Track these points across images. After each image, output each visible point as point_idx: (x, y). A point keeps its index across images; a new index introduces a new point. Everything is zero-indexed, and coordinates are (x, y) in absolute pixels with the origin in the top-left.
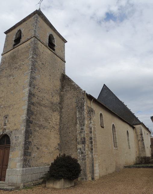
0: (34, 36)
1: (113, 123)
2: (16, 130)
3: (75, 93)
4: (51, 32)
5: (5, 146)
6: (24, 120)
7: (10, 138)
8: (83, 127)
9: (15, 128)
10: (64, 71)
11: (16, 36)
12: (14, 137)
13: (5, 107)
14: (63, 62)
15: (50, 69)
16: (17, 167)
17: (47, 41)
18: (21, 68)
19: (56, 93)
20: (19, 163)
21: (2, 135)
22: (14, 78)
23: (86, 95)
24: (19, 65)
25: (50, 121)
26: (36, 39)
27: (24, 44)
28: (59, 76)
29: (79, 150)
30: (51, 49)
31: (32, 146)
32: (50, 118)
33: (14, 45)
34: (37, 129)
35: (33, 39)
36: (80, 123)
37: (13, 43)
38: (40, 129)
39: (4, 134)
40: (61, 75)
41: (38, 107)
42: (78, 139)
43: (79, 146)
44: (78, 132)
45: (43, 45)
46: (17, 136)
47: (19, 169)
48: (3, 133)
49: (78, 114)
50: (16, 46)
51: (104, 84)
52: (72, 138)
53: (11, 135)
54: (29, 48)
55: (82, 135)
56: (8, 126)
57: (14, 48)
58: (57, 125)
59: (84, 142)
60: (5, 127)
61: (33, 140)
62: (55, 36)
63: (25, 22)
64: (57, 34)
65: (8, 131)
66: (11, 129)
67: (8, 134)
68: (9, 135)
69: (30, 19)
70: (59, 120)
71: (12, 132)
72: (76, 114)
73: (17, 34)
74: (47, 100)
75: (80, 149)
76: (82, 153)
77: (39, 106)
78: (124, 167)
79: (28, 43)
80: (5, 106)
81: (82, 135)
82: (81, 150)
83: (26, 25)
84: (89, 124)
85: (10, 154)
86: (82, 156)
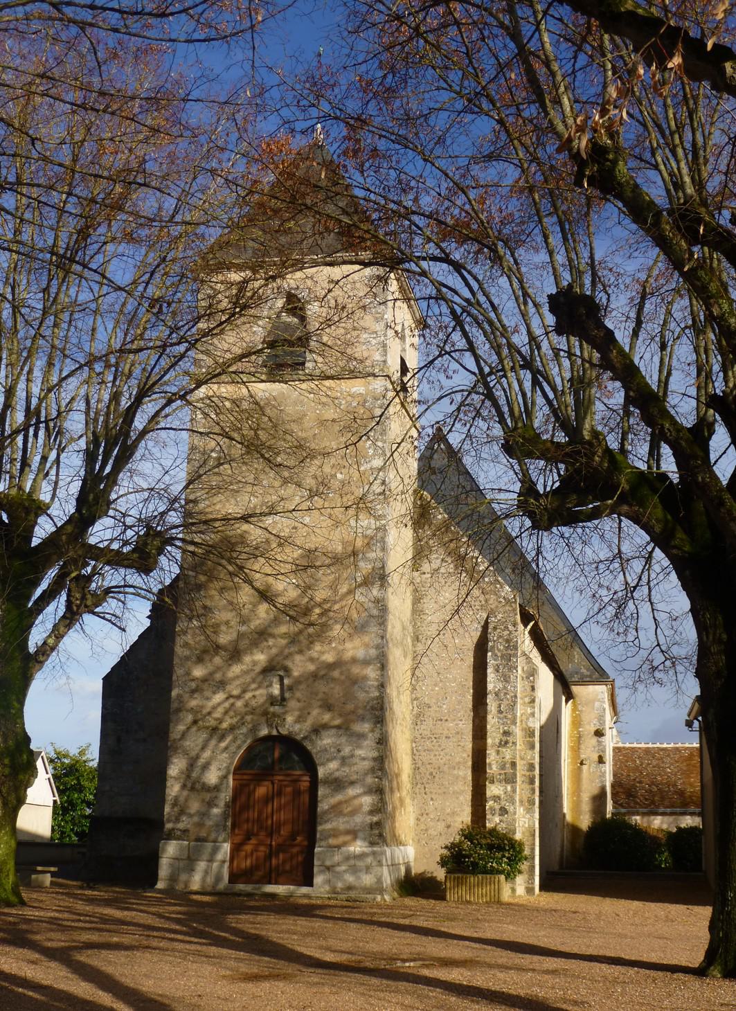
36: (500, 712)
84: (528, 719)
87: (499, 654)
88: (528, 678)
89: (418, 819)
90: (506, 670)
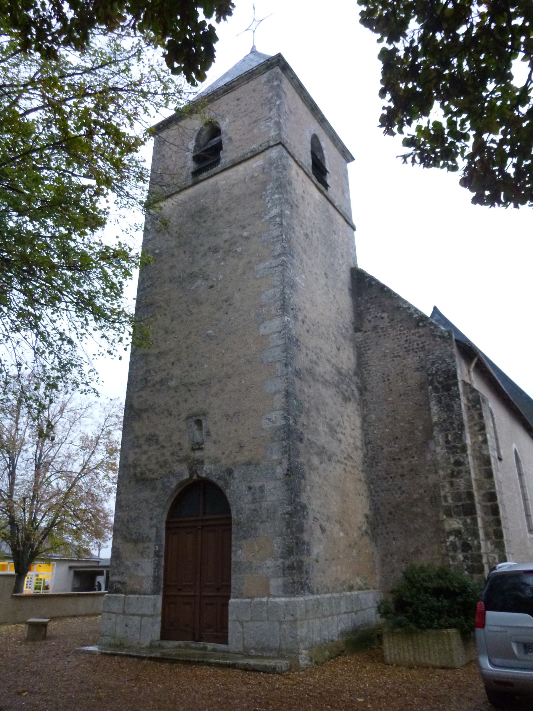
0: (280, 143)
1: (514, 446)
2: (249, 464)
3: (414, 338)
4: (315, 128)
5: (202, 520)
6: (280, 429)
7: (227, 493)
9: (246, 455)
10: (355, 259)
11: (197, 140)
13: (185, 385)
14: (350, 229)
15: (323, 254)
16: (272, 591)
17: (307, 160)
18: (239, 250)
19: (344, 337)
20: (280, 581)
21: (187, 480)
22: (210, 283)
23: (454, 344)
24: (226, 241)
25: (340, 436)
26: (285, 153)
27: (241, 168)
28: (345, 277)
30: (320, 185)
31: (311, 521)
32: (338, 425)
33: (196, 173)
34: (316, 461)
35: (274, 153)
36: (447, 442)
37: (191, 165)
38: (321, 463)
39: (195, 477)
40: (349, 274)
41: (310, 387)
42: (445, 497)
43: (455, 523)
44: (441, 473)
45: (301, 172)
47: (283, 599)
48: (191, 476)
50: (205, 175)
51: (435, 308)
52: (415, 496)
53: (227, 484)
54: (264, 184)
57: (195, 184)
58: (356, 449)
60: (198, 454)
61: (309, 498)
62: (325, 143)
63: (232, 95)
64: (327, 134)
65: (213, 467)
66: (223, 462)
67: (214, 479)
68: (221, 483)
69: (253, 84)
70: (359, 431)
71: (230, 472)
72: (429, 409)
73: (200, 133)
74: (329, 361)
75: (457, 533)
76: (466, 547)
77: (312, 383)
79: (254, 165)
80: (186, 380)
82: (460, 539)
83: (238, 105)
84: (480, 447)
85: (233, 549)
86: (466, 558)
87: (439, 386)
88: (474, 406)
89: (383, 561)
90: (448, 400)
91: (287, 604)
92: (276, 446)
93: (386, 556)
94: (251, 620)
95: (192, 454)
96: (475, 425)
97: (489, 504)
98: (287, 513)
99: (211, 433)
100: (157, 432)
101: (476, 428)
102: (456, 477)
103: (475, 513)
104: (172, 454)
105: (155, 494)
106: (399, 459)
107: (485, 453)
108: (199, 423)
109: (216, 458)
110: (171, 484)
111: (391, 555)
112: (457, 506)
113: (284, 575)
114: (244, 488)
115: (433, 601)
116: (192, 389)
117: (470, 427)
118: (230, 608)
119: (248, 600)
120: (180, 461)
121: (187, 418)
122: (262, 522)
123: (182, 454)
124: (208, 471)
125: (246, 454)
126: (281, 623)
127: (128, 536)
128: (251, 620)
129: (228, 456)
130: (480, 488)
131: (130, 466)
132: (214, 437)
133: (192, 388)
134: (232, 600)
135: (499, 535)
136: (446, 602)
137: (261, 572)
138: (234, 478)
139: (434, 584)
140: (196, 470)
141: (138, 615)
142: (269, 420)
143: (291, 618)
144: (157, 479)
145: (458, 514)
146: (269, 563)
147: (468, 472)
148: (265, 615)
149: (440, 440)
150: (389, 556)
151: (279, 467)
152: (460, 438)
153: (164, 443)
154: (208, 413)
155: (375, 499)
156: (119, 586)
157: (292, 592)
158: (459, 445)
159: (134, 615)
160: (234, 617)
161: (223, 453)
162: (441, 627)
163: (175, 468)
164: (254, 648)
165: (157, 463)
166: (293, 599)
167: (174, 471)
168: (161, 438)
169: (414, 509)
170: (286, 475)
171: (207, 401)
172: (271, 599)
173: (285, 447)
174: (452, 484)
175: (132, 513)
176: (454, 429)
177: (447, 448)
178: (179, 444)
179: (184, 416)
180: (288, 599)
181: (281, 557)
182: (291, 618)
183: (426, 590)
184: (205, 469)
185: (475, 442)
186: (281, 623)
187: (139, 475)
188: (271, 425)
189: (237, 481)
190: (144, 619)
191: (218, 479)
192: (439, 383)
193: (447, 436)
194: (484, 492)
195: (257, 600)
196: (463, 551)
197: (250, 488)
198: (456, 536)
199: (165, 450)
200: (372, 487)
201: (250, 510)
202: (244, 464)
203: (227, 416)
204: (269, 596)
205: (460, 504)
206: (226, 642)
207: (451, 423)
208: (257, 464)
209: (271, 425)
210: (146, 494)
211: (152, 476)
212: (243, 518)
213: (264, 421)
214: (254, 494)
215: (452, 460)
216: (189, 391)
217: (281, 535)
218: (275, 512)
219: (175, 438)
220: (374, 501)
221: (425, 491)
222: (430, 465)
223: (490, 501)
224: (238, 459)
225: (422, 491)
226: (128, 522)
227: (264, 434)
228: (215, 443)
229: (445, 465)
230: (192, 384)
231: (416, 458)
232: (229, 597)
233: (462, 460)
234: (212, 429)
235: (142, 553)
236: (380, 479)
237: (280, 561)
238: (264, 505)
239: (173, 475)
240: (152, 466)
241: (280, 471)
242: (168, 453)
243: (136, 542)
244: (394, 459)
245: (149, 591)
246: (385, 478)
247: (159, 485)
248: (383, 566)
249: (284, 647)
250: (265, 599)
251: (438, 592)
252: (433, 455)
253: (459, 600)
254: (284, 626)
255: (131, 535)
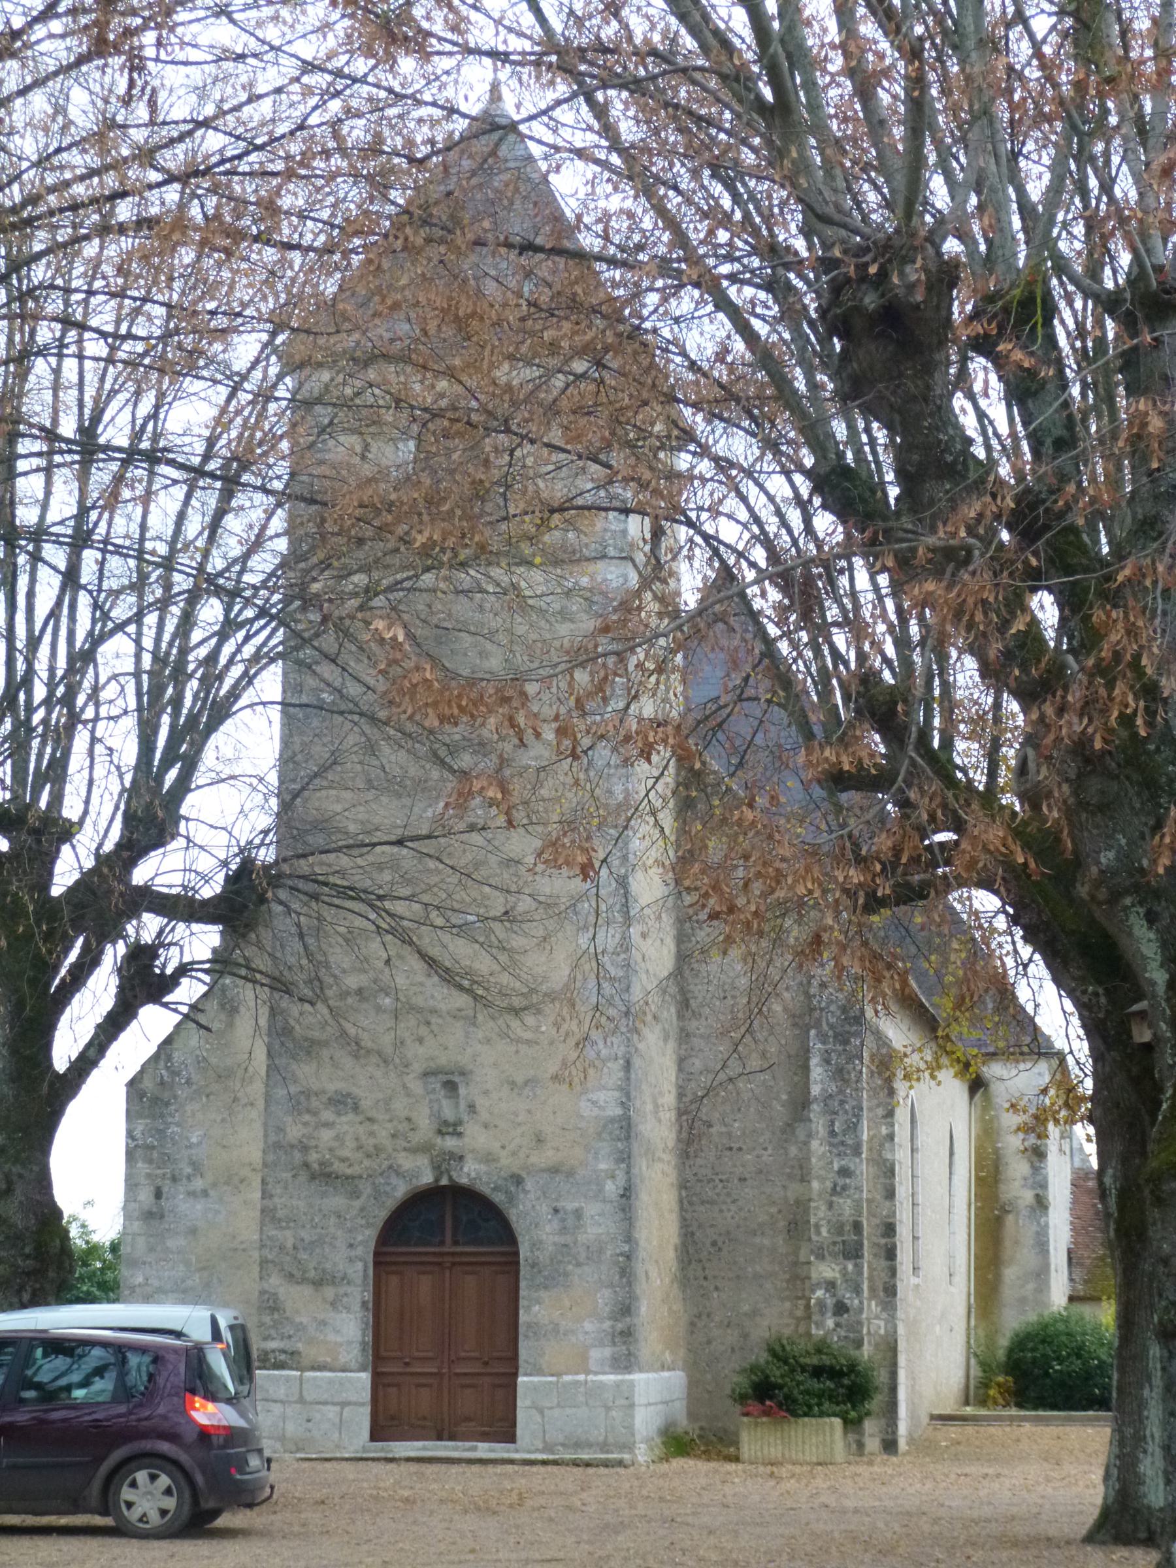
2: (554, 1170)
5: (453, 1254)
6: (612, 1120)
7: (513, 1215)
8: (848, 1162)
12: (544, 1209)
16: (592, 1366)
20: (607, 1352)
29: (820, 1293)
36: (832, 1133)
42: (817, 1226)
43: (827, 1270)
44: (815, 1185)
46: (570, 1205)
47: (612, 1377)
49: (817, 1071)
53: (511, 1199)
55: (846, 1206)
56: (475, 1137)
59: (853, 1252)
60: (450, 1143)
65: (483, 1168)
67: (486, 1190)
68: (498, 1198)
71: (518, 1180)
75: (831, 1285)
76: (841, 1308)
78: (933, 1417)
81: (846, 1206)
84: (882, 1145)
86: (837, 1325)
89: (693, 1324)
91: (618, 1385)
92: (605, 1148)
93: (699, 1316)
94: (558, 1405)
95: (439, 1140)
96: (878, 1106)
97: (883, 1241)
98: (621, 1254)
99: (478, 1108)
100: (356, 1091)
101: (880, 1112)
102: (840, 1194)
103: (862, 1257)
104: (394, 1136)
105: (357, 1204)
106: (740, 1149)
107: (889, 1156)
108: (451, 1087)
109: (490, 1154)
110: (394, 1188)
111: (709, 1315)
112: (834, 1243)
113: (614, 1344)
114: (545, 1208)
115: (815, 1385)
116: (433, 1021)
117: (870, 1109)
118: (520, 1391)
119: (554, 1379)
120: (414, 1150)
121: (425, 1074)
122: (579, 1265)
123: (417, 1138)
124: (473, 1175)
125: (550, 1153)
126: (608, 1409)
127: (298, 1274)
128: (558, 1405)
129: (514, 1154)
130: (871, 1214)
131: (292, 1146)
132: (484, 1115)
133: (434, 1020)
134: (521, 1379)
135: (891, 1291)
136: (830, 1384)
137: (573, 1339)
138: (526, 1192)
139: (814, 1360)
140: (448, 1171)
141: (334, 1404)
142: (594, 1103)
143: (624, 1402)
144: (360, 1177)
145: (834, 1255)
146: (588, 1326)
147: (859, 1189)
148: (581, 1399)
149: (821, 1129)
150: (704, 1317)
151: (609, 1182)
152: (853, 1127)
153: (373, 1114)
154: (471, 1072)
155: (688, 1216)
156: (283, 1357)
157: (626, 1368)
158: (850, 1142)
159: (325, 1403)
160: (528, 1403)
161: (503, 1147)
162: (822, 1414)
163: (401, 1161)
164: (563, 1445)
165: (360, 1148)
166: (627, 1377)
167: (400, 1166)
168: (365, 1104)
169: (758, 1240)
170: (622, 1196)
171: (469, 1050)
172: (591, 1377)
173: (622, 1152)
174: (830, 1205)
175: (303, 1234)
176: (846, 1112)
177: (831, 1145)
178: (409, 1119)
179: (418, 1067)
180: (620, 1377)
181: (610, 1319)
182: (624, 1402)
183: (803, 1369)
184: (466, 1170)
185: (874, 1136)
186: (608, 1409)
187: (316, 1166)
188: (596, 1112)
189: (531, 1196)
190: (347, 1409)
191: (494, 1189)
192: (831, 1027)
193: (832, 1123)
194: (878, 1221)
195: (568, 1378)
196: (835, 1314)
197: (556, 1211)
198: (827, 1290)
199: (375, 1127)
200: (684, 1194)
201: (555, 1244)
202: (543, 1170)
203: (513, 1084)
204: (588, 1372)
205: (839, 1239)
206: (509, 1437)
207: (842, 1102)
208: (570, 1174)
209: (596, 1112)
210: (336, 1201)
211: (349, 1171)
212: (543, 1257)
213: (583, 1104)
214: (563, 1220)
215: (836, 1167)
216: (428, 1023)
217: (611, 1285)
218: (601, 1251)
219: (400, 1106)
220: (685, 1219)
221: (780, 1211)
222: (793, 1167)
223: (883, 1236)
224: (533, 1159)
225: (774, 1210)
226: (295, 1248)
227: (583, 1125)
228: (486, 1126)
229: (822, 1172)
230: (433, 1011)
231: (770, 1151)
232: (515, 1375)
233: (852, 1167)
234: (481, 1102)
235: (332, 1304)
236: (699, 1181)
237: (607, 1324)
238: (582, 1238)
239: (398, 1174)
240: (345, 1153)
241: (611, 1188)
242: (384, 1133)
243: (318, 1283)
244: (731, 1149)
245: (353, 1365)
246: (710, 1181)
247: (367, 1189)
248: (692, 1332)
249: (611, 1440)
250: (581, 1377)
251: (818, 1372)
252: (800, 1150)
253: (846, 1381)
254: (614, 1413)
255: (304, 1272)
